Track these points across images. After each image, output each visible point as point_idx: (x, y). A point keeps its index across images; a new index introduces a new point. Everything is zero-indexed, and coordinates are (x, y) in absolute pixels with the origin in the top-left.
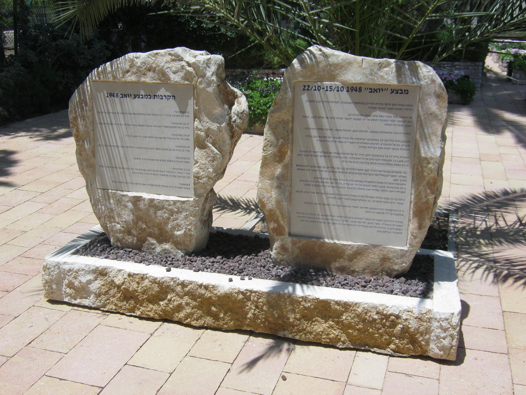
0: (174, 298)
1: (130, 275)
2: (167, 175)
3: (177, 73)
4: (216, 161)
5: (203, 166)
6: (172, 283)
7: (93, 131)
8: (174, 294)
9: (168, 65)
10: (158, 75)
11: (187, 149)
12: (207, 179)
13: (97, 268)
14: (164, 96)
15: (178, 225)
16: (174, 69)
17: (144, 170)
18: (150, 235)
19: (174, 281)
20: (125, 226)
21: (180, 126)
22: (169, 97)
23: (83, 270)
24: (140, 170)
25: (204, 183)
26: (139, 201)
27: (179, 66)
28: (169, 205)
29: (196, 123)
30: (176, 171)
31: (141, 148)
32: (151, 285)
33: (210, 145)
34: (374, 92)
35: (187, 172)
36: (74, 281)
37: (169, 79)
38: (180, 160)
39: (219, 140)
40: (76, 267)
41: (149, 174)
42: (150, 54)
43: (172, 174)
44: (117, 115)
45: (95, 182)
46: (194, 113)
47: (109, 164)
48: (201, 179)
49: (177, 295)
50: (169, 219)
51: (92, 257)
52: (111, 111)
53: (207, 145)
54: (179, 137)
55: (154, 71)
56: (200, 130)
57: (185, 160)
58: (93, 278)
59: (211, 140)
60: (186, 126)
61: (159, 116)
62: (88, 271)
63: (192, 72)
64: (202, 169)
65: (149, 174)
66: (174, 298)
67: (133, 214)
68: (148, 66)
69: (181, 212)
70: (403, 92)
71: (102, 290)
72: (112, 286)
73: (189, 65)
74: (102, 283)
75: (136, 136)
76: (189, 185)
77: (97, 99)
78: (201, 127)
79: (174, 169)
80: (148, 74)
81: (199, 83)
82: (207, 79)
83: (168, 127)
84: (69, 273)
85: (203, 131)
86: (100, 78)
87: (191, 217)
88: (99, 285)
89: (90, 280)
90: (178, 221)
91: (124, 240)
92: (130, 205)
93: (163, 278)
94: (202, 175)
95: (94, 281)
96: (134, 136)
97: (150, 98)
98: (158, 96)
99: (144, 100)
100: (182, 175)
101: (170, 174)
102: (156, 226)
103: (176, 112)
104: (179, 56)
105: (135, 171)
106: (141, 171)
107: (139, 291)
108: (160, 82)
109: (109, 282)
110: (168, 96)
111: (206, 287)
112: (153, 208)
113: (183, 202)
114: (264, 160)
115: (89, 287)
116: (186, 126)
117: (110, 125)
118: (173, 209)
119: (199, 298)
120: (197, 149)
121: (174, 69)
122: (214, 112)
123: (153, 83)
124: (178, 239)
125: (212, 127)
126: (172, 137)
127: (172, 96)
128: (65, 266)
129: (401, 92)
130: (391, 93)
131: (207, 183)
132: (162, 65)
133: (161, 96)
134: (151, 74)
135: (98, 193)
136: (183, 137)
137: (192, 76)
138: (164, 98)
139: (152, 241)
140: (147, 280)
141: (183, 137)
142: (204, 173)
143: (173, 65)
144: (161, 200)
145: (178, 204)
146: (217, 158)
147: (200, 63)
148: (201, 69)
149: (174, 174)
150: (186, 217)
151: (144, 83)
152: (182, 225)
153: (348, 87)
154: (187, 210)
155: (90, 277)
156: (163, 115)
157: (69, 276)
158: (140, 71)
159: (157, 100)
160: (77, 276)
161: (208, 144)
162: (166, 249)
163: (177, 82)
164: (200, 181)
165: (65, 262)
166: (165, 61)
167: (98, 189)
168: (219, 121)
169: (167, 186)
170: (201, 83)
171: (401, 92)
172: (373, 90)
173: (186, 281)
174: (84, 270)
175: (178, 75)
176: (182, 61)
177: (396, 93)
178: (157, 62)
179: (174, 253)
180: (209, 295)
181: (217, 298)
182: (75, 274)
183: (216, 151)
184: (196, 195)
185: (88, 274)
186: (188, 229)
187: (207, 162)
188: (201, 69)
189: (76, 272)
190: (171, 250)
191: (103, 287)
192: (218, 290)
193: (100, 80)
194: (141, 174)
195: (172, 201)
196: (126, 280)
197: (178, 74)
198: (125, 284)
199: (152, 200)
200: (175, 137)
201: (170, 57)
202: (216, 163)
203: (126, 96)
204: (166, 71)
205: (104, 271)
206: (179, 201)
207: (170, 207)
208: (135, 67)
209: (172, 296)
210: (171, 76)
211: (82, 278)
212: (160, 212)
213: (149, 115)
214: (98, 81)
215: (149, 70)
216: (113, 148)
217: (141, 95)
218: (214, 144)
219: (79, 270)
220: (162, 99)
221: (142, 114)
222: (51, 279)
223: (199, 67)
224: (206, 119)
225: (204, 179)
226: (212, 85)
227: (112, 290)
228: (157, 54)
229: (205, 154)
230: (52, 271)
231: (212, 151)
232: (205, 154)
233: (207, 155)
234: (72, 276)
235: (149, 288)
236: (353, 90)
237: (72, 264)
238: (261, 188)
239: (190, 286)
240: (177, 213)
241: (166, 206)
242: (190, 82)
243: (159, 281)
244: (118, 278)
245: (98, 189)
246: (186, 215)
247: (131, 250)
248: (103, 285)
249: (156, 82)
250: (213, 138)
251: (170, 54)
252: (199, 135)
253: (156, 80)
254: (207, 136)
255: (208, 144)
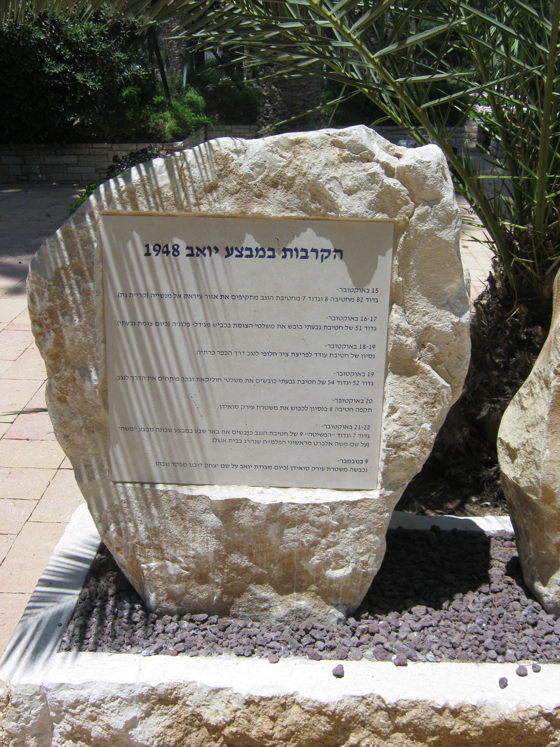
0: (367, 740)
1: (249, 703)
2: (309, 443)
3: (355, 192)
4: (440, 404)
5: (409, 419)
6: (362, 708)
7: (104, 341)
8: (366, 732)
9: (331, 172)
10: (299, 197)
11: (366, 379)
12: (419, 447)
13: (153, 689)
14: (313, 250)
15: (338, 556)
16: (348, 183)
17: (247, 433)
18: (259, 580)
19: (368, 704)
20: (193, 566)
21: (353, 324)
22: (326, 254)
23: (114, 699)
24: (234, 432)
25: (412, 459)
26: (238, 509)
27: (362, 175)
28: (322, 514)
29: (396, 317)
30: (332, 431)
31: (240, 380)
32: (309, 719)
33: (428, 367)
34: (198, 255)
35: (363, 432)
36: (88, 725)
37: (335, 208)
38: (346, 405)
39: (449, 355)
40: (95, 695)
41: (258, 442)
42: (276, 143)
43: (323, 439)
44: (184, 301)
45: (106, 467)
46: (391, 291)
47: (156, 421)
48: (404, 450)
49: (376, 732)
50: (315, 544)
51: (118, 651)
52: (165, 289)
53: (418, 368)
54: (347, 351)
55: (288, 188)
56: (404, 332)
57: (360, 406)
58: (141, 712)
59: (430, 355)
60: (368, 323)
61: (293, 302)
62: (127, 700)
63: (399, 191)
64: (407, 426)
65: (258, 442)
66: (367, 740)
67: (218, 538)
68: (272, 175)
69: (345, 527)
70: (254, 253)
71: (168, 739)
72: (192, 726)
73: (389, 171)
74: (168, 723)
75: (227, 353)
76: (367, 461)
77: (125, 259)
78: (409, 326)
79: (329, 427)
80: (271, 195)
81: (418, 219)
82: (443, 208)
83: (319, 328)
84: (74, 708)
85: (411, 335)
86: (135, 206)
87: (371, 536)
88: (159, 729)
89: (135, 718)
90: (338, 548)
91: (187, 596)
92: (212, 520)
93: (341, 702)
94: (409, 440)
95: (144, 718)
96: (222, 353)
97: (273, 256)
98: (296, 250)
99: (255, 261)
100: (348, 440)
101: (318, 438)
102: (277, 561)
103: (344, 290)
104: (363, 148)
105: (219, 436)
106: (238, 437)
107: (277, 735)
108: (304, 215)
109: (186, 718)
110: (323, 250)
111: (455, 713)
112: (276, 525)
113: (354, 504)
114: (556, 396)
115: (131, 736)
116: (368, 323)
117: (163, 328)
118: (330, 523)
119: (433, 733)
120: (391, 378)
121: (350, 183)
122: (446, 289)
123: (284, 218)
124: (334, 585)
125: (438, 325)
126: (328, 351)
127: (336, 251)
128: (63, 693)
129: (248, 253)
130: (226, 257)
131: (418, 458)
132: (315, 171)
133: (303, 250)
134: (279, 195)
135: (117, 491)
136: (358, 351)
137: (399, 201)
138: (312, 255)
139: (264, 594)
140: (295, 708)
141: (358, 351)
142: (412, 434)
143: (346, 172)
144: (299, 505)
145: (342, 510)
146: (443, 397)
147: (428, 167)
148: (429, 182)
149: (328, 439)
150: (358, 537)
151: (260, 218)
152: (348, 555)
153: (147, 246)
154: (360, 521)
155: (134, 712)
156: (307, 299)
157: (73, 715)
158: (248, 187)
159: (292, 262)
160: (98, 714)
161: (423, 364)
162: (300, 610)
163: (356, 215)
164: (401, 453)
165: (61, 685)
166: (324, 162)
167: (115, 483)
168: (456, 310)
169: (307, 468)
170: (423, 218)
171: (248, 253)
172: (195, 251)
173: (402, 703)
174: (118, 697)
175: (360, 199)
176: (368, 161)
177: (237, 256)
178: (298, 163)
179: (321, 615)
180: (463, 728)
181: (481, 732)
182: (92, 712)
183: (442, 382)
184: (386, 485)
185: (127, 705)
186: (362, 561)
187: (416, 407)
188: (429, 182)
189: (94, 705)
190: (313, 611)
191: (170, 732)
192: (483, 715)
193: (124, 212)
194: (239, 441)
195: (327, 504)
196: (238, 713)
197: (359, 194)
198: (235, 724)
199: (276, 508)
200: (337, 351)
201: (337, 150)
202: (440, 408)
203: (201, 251)
204: (327, 186)
205: (171, 694)
206: (343, 503)
207: (323, 519)
208: (231, 176)
209: (361, 735)
210: (339, 201)
211: (113, 719)
212: (294, 530)
213: (267, 298)
214: (122, 215)
215: (274, 185)
216: (170, 385)
217: (247, 249)
218: (434, 365)
219: (103, 701)
220: (306, 257)
221: (246, 297)
222: (23, 728)
223: (425, 178)
224: (423, 304)
225: (413, 449)
226: (453, 223)
227: (193, 735)
228: (298, 142)
229: (412, 389)
230: (26, 709)
231: (433, 382)
232: (412, 389)
233: (419, 391)
234: (85, 715)
235: (304, 726)
236: (159, 251)
237: (82, 687)
238: (550, 461)
239: (414, 712)
240: (337, 529)
241: (312, 517)
242: (389, 216)
243: (334, 712)
244: (213, 708)
245: (115, 483)
246: (359, 532)
247: (205, 616)
248: (170, 727)
249: (294, 214)
250: (436, 350)
251: (335, 144)
252: (401, 345)
253: (292, 211)
254: (421, 345)
255: (423, 364)
